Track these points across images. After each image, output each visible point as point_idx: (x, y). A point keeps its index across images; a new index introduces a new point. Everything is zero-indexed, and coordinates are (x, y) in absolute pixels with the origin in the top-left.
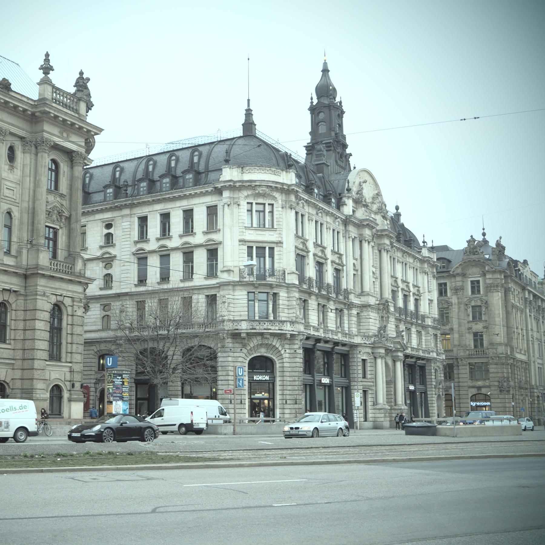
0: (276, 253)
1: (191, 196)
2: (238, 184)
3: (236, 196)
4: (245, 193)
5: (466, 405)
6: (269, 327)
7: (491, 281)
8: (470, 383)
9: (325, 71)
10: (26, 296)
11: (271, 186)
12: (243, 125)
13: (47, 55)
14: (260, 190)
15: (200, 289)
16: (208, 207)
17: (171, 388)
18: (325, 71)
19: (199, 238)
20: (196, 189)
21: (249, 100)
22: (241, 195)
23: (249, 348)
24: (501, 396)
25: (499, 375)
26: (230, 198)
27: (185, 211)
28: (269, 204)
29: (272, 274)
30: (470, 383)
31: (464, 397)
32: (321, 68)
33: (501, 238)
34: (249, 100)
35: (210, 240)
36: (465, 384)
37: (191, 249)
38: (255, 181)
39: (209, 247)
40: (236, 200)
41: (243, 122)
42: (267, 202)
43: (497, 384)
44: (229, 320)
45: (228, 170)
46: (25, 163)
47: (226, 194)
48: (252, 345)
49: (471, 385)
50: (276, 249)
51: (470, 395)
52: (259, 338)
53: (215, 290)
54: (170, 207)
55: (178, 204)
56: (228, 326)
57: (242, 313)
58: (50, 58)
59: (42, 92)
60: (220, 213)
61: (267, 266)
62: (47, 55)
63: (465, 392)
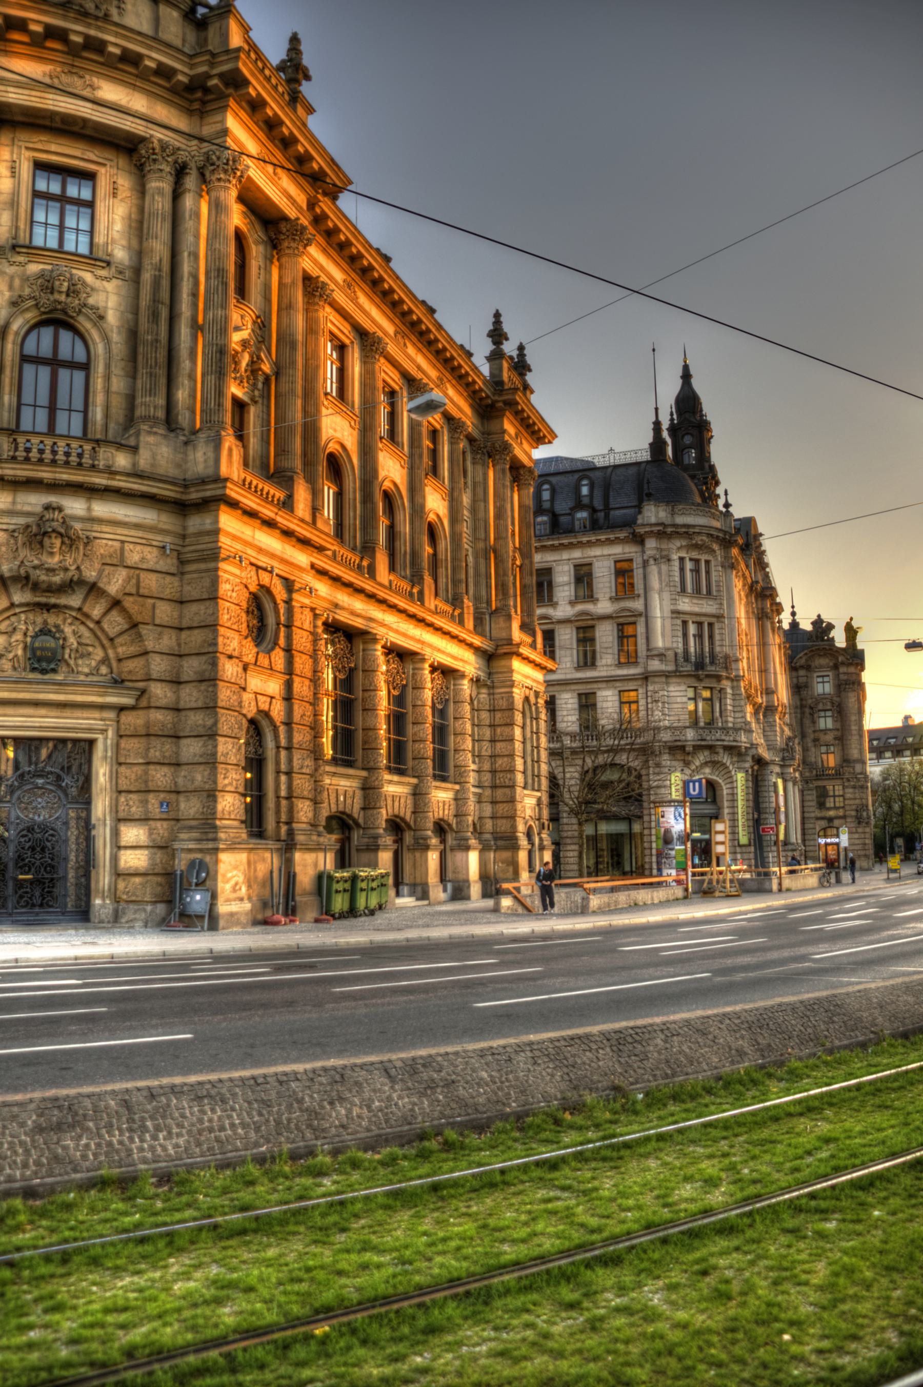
0: (717, 631)
1: (590, 544)
2: (669, 530)
3: (664, 546)
4: (678, 543)
5: (812, 843)
6: (723, 737)
7: (845, 677)
8: (818, 814)
9: (686, 376)
10: (493, 687)
11: (712, 535)
12: (651, 445)
13: (497, 315)
14: (698, 539)
15: (610, 681)
16: (575, 566)
17: (566, 828)
18: (686, 376)
19: (604, 606)
20: (553, 539)
21: (657, 409)
22: (671, 546)
23: (693, 767)
24: (860, 830)
25: (857, 802)
26: (657, 549)
27: (577, 567)
28: (691, 559)
29: (712, 662)
30: (818, 814)
31: (810, 831)
32: (680, 373)
33: (851, 619)
34: (657, 409)
35: (623, 610)
36: (813, 815)
37: (590, 623)
38: (694, 526)
39: (621, 620)
40: (664, 553)
41: (651, 440)
42: (703, 557)
43: (854, 813)
44: (666, 728)
45: (653, 508)
46: (477, 479)
47: (651, 543)
48: (698, 763)
49: (819, 815)
50: (717, 626)
51: (818, 829)
52: (707, 753)
53: (635, 683)
54: (552, 558)
55: (565, 555)
56: (666, 736)
57: (682, 717)
58: (502, 319)
59: (496, 372)
60: (638, 573)
61: (707, 649)
62: (497, 315)
63: (811, 826)
